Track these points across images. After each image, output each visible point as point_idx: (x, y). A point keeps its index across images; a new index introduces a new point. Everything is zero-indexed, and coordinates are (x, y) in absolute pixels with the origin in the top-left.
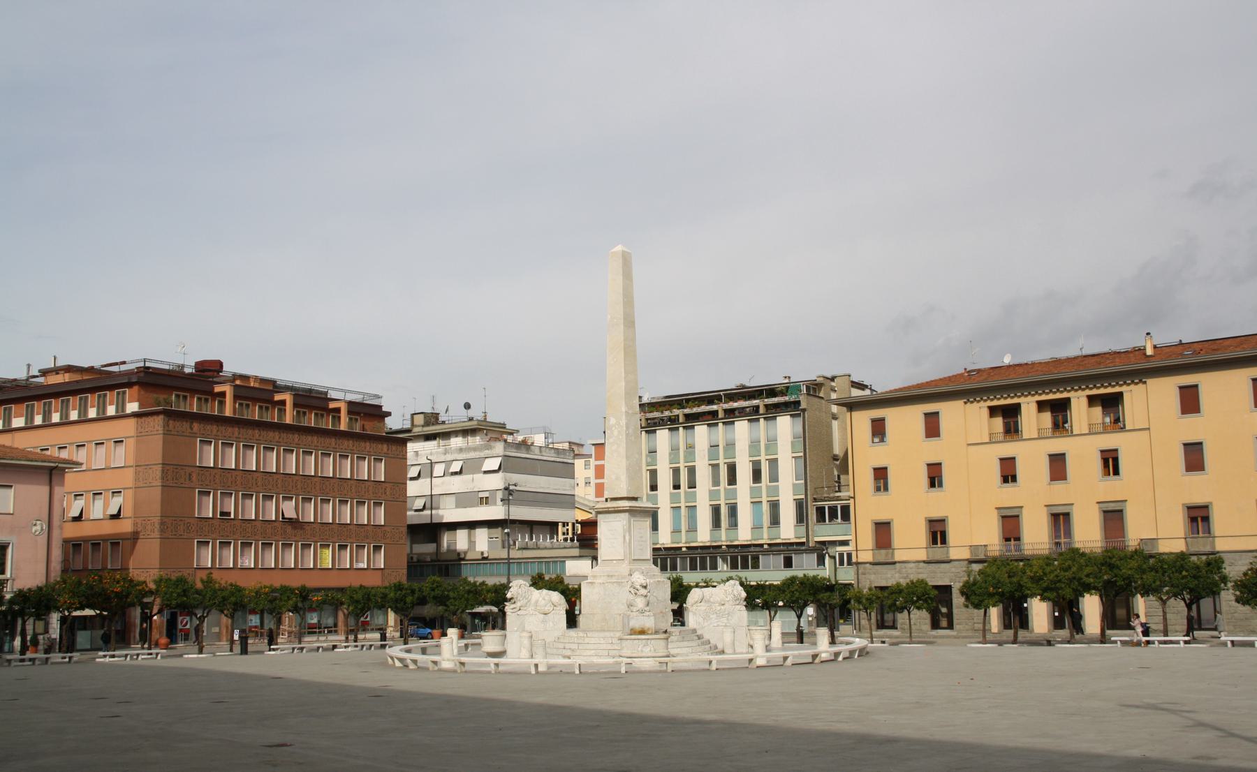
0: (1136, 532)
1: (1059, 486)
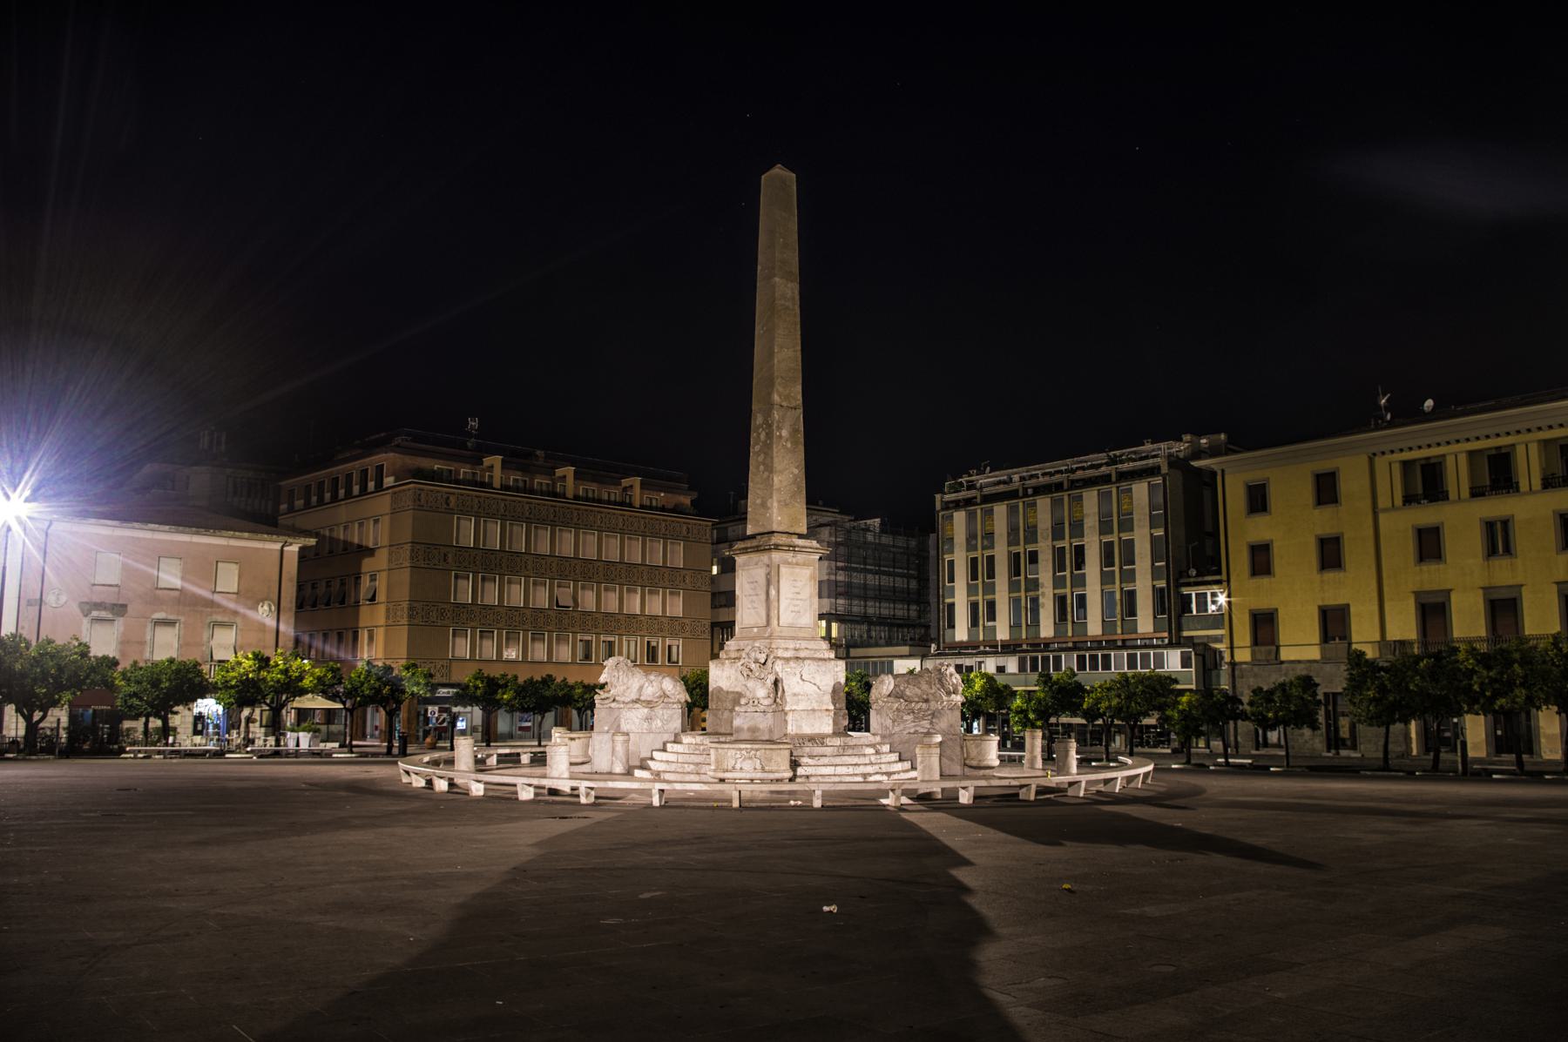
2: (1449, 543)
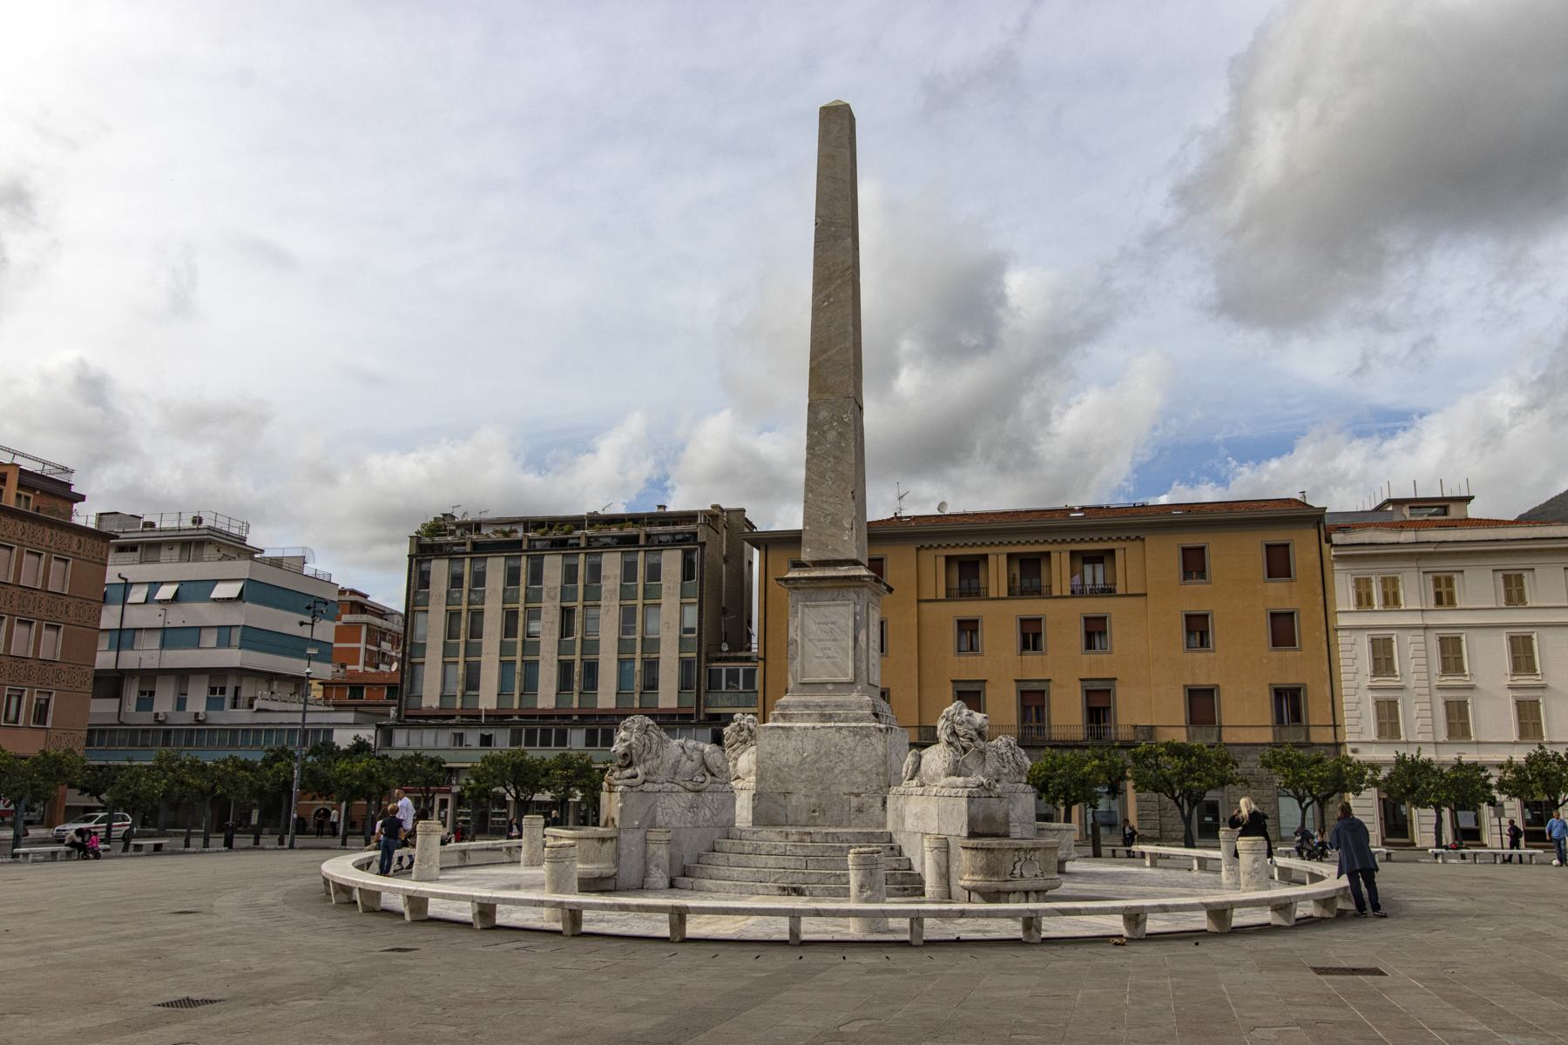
0: (1129, 714)
1: (1031, 658)
2: (986, 635)
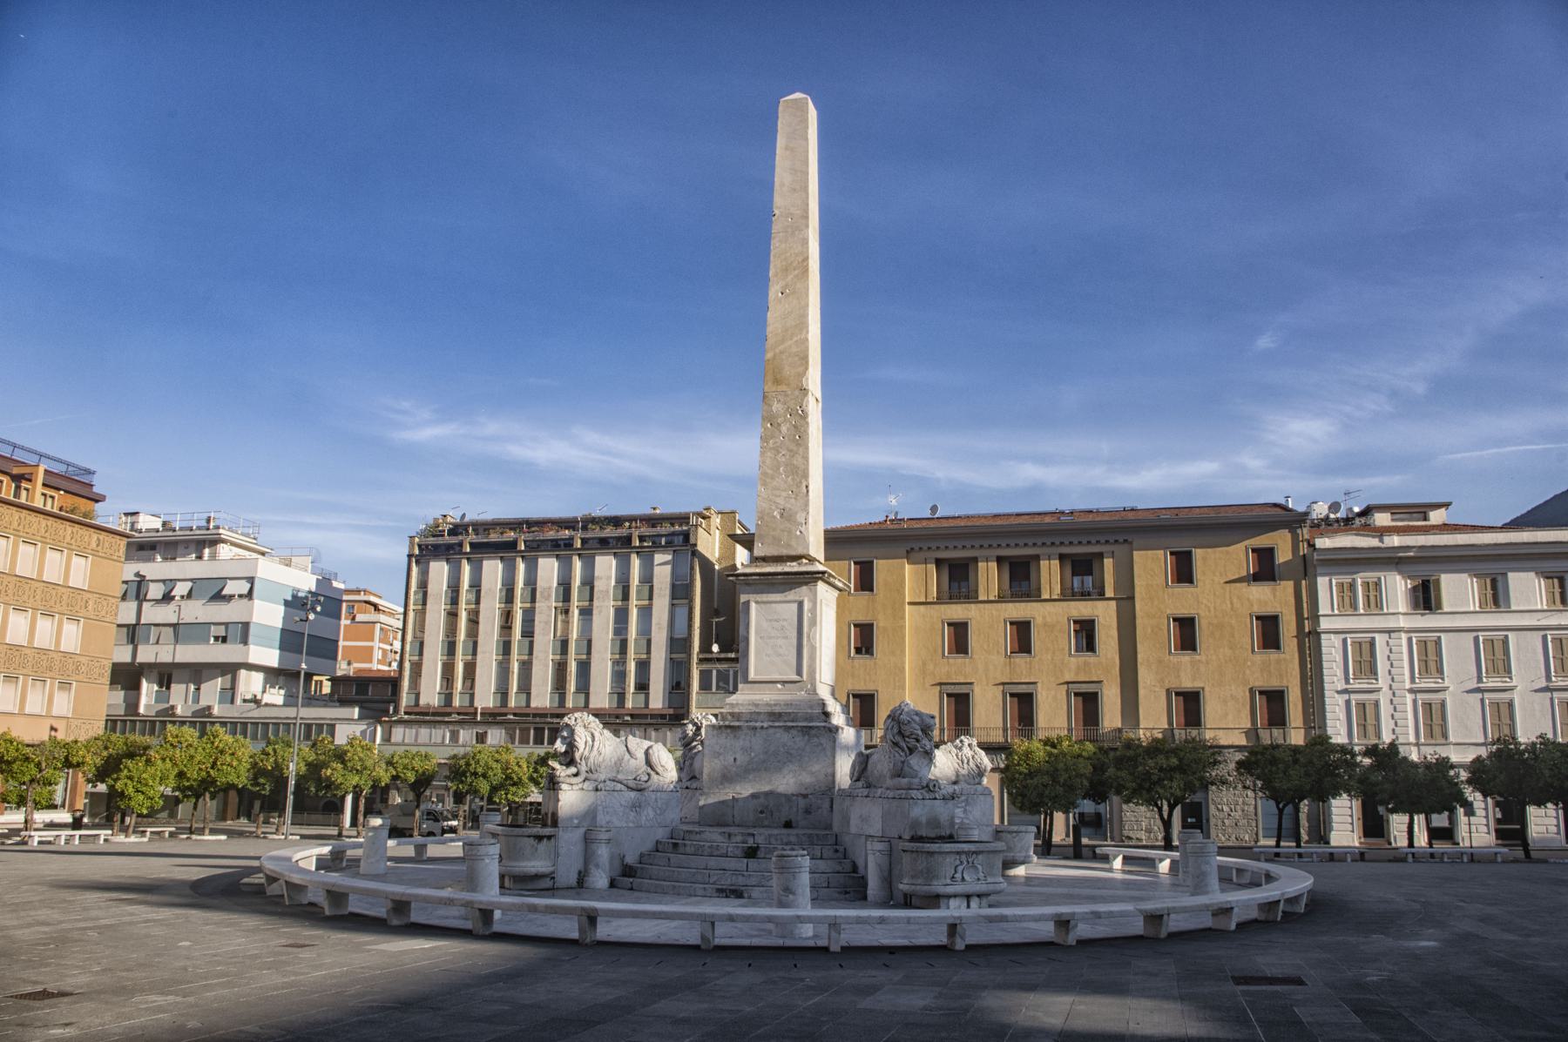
1: (1021, 660)
